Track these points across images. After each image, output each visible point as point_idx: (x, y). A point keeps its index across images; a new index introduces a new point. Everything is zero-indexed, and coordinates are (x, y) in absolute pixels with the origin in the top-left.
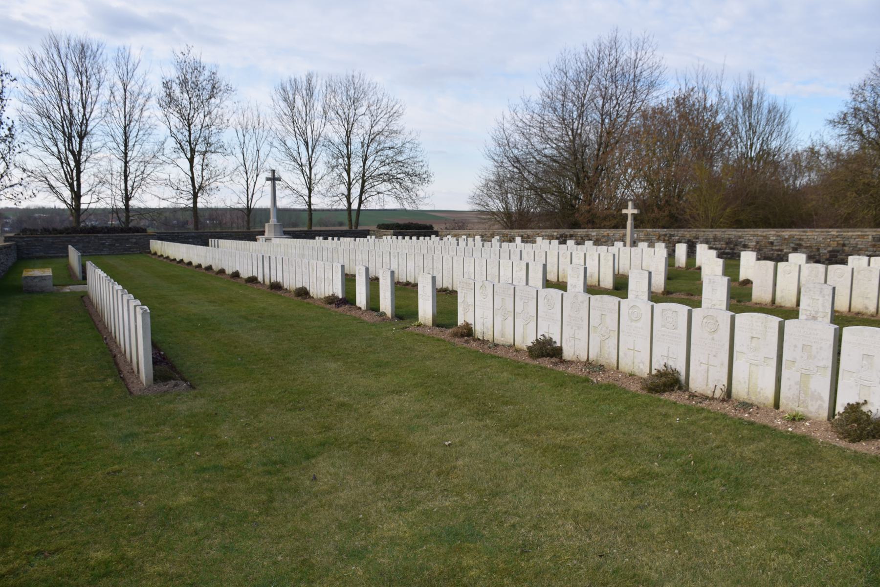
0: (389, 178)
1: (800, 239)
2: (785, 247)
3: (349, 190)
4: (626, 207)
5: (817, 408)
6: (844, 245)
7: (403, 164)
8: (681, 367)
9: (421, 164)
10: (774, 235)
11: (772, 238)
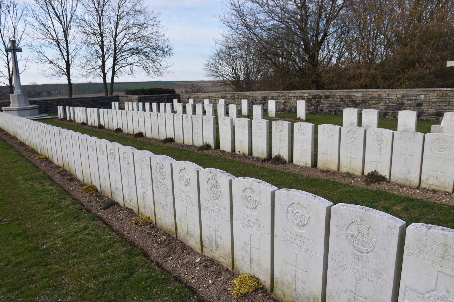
0: (136, 51)
3: (104, 62)
5: (356, 169)
7: (147, 39)
9: (163, 38)
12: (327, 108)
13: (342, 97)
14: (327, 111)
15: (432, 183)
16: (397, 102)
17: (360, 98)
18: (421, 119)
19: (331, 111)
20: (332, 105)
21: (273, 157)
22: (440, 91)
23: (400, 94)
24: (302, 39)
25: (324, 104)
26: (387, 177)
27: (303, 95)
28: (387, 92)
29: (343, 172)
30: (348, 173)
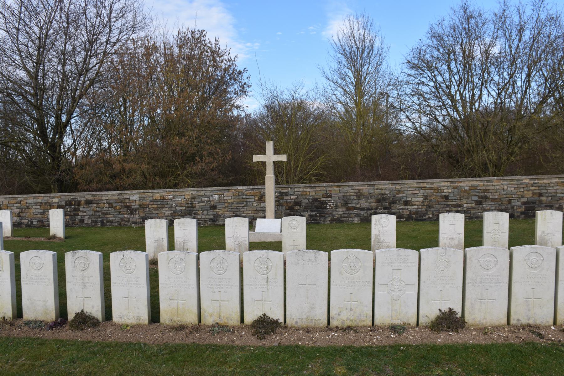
1: (485, 191)
2: (465, 201)
4: (263, 151)
6: (541, 195)
8: (458, 309)
10: (448, 187)
11: (446, 191)
12: (89, 218)
13: (111, 202)
14: (90, 221)
15: (345, 318)
16: (186, 205)
17: (137, 202)
18: (217, 225)
19: (96, 222)
20: (97, 214)
21: (71, 316)
22: (235, 190)
23: (189, 195)
24: (37, 120)
25: (85, 212)
26: (281, 320)
27: (51, 200)
28: (172, 193)
29: (207, 324)
30: (217, 323)
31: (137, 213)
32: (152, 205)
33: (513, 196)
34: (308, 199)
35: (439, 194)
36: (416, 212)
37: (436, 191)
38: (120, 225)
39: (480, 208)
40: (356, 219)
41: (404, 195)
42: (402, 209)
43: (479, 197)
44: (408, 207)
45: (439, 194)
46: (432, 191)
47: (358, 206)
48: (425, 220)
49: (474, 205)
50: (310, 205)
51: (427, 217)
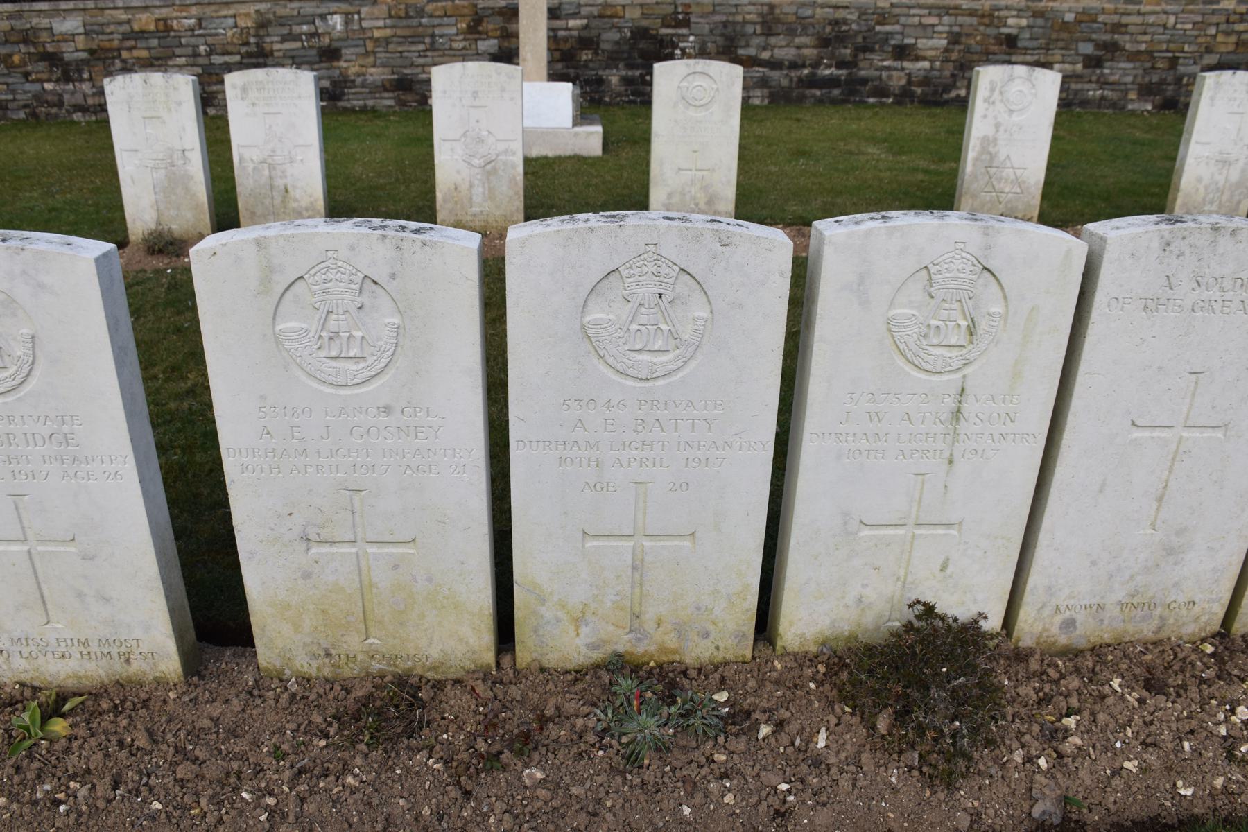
1: (1118, 28)
16: (243, 50)
18: (345, 109)
23: (247, 15)
31: (86, 76)
32: (130, 49)
33: (1186, 48)
34: (620, 29)
35: (992, 31)
36: (926, 81)
37: (986, 21)
38: (34, 115)
39: (1094, 78)
40: (758, 92)
41: (897, 28)
42: (888, 68)
43: (1098, 46)
44: (906, 64)
45: (992, 31)
46: (974, 20)
47: (765, 55)
48: (947, 102)
49: (1079, 67)
50: (626, 47)
51: (953, 94)
